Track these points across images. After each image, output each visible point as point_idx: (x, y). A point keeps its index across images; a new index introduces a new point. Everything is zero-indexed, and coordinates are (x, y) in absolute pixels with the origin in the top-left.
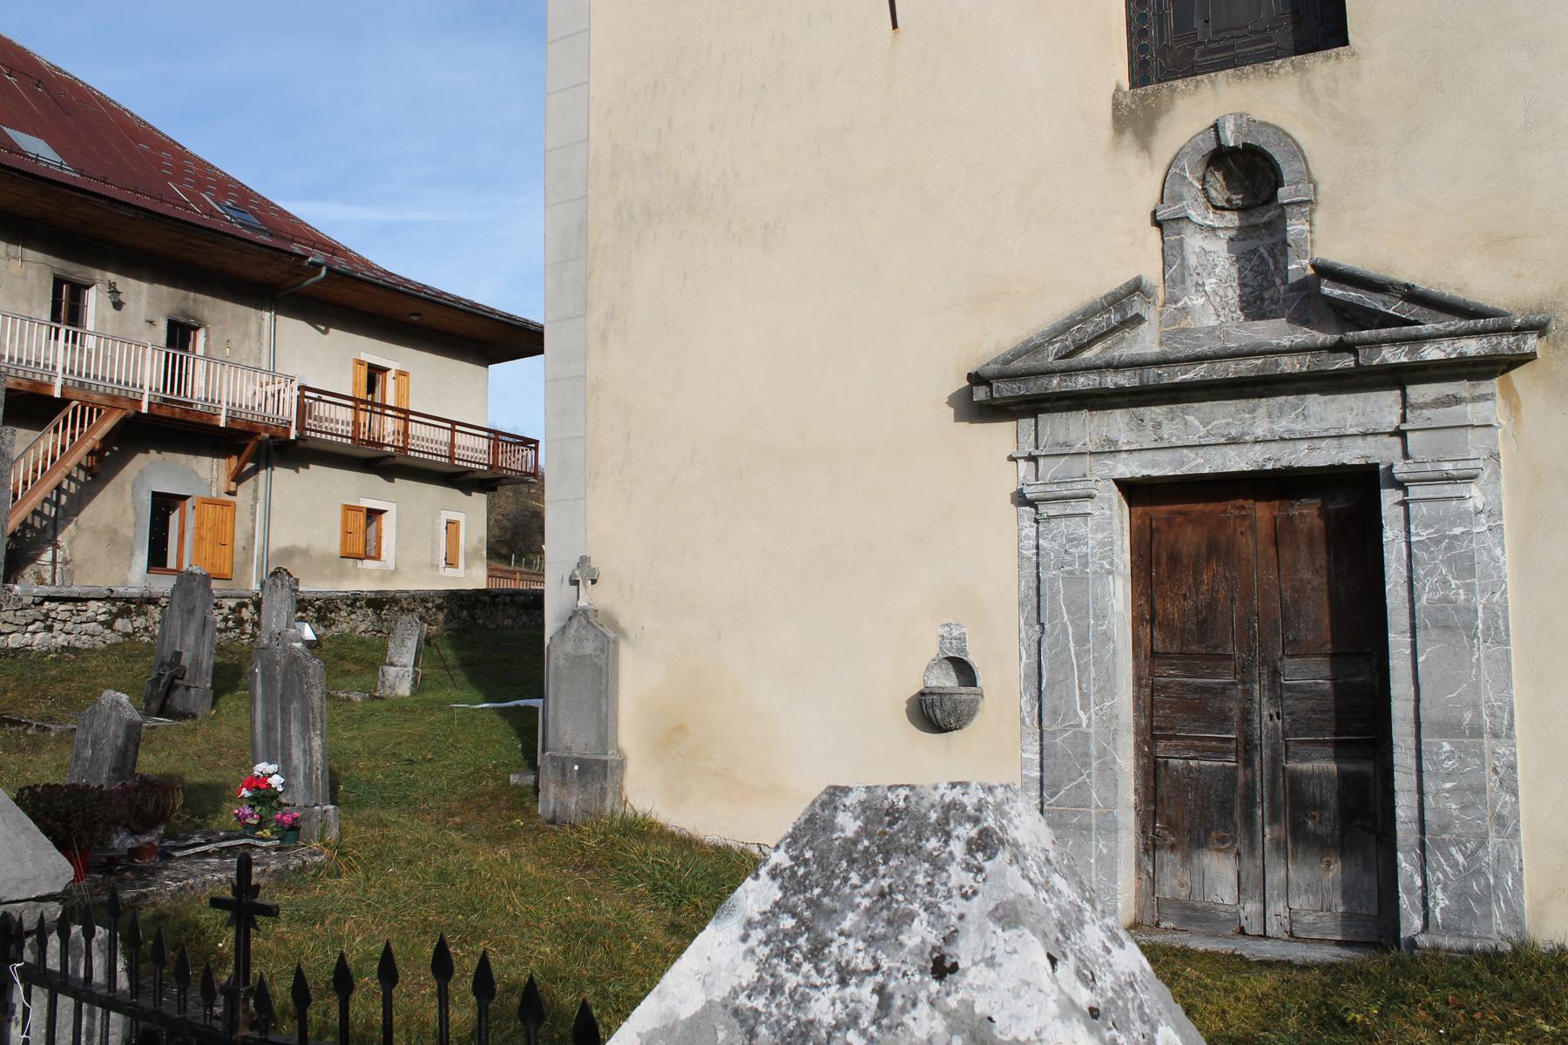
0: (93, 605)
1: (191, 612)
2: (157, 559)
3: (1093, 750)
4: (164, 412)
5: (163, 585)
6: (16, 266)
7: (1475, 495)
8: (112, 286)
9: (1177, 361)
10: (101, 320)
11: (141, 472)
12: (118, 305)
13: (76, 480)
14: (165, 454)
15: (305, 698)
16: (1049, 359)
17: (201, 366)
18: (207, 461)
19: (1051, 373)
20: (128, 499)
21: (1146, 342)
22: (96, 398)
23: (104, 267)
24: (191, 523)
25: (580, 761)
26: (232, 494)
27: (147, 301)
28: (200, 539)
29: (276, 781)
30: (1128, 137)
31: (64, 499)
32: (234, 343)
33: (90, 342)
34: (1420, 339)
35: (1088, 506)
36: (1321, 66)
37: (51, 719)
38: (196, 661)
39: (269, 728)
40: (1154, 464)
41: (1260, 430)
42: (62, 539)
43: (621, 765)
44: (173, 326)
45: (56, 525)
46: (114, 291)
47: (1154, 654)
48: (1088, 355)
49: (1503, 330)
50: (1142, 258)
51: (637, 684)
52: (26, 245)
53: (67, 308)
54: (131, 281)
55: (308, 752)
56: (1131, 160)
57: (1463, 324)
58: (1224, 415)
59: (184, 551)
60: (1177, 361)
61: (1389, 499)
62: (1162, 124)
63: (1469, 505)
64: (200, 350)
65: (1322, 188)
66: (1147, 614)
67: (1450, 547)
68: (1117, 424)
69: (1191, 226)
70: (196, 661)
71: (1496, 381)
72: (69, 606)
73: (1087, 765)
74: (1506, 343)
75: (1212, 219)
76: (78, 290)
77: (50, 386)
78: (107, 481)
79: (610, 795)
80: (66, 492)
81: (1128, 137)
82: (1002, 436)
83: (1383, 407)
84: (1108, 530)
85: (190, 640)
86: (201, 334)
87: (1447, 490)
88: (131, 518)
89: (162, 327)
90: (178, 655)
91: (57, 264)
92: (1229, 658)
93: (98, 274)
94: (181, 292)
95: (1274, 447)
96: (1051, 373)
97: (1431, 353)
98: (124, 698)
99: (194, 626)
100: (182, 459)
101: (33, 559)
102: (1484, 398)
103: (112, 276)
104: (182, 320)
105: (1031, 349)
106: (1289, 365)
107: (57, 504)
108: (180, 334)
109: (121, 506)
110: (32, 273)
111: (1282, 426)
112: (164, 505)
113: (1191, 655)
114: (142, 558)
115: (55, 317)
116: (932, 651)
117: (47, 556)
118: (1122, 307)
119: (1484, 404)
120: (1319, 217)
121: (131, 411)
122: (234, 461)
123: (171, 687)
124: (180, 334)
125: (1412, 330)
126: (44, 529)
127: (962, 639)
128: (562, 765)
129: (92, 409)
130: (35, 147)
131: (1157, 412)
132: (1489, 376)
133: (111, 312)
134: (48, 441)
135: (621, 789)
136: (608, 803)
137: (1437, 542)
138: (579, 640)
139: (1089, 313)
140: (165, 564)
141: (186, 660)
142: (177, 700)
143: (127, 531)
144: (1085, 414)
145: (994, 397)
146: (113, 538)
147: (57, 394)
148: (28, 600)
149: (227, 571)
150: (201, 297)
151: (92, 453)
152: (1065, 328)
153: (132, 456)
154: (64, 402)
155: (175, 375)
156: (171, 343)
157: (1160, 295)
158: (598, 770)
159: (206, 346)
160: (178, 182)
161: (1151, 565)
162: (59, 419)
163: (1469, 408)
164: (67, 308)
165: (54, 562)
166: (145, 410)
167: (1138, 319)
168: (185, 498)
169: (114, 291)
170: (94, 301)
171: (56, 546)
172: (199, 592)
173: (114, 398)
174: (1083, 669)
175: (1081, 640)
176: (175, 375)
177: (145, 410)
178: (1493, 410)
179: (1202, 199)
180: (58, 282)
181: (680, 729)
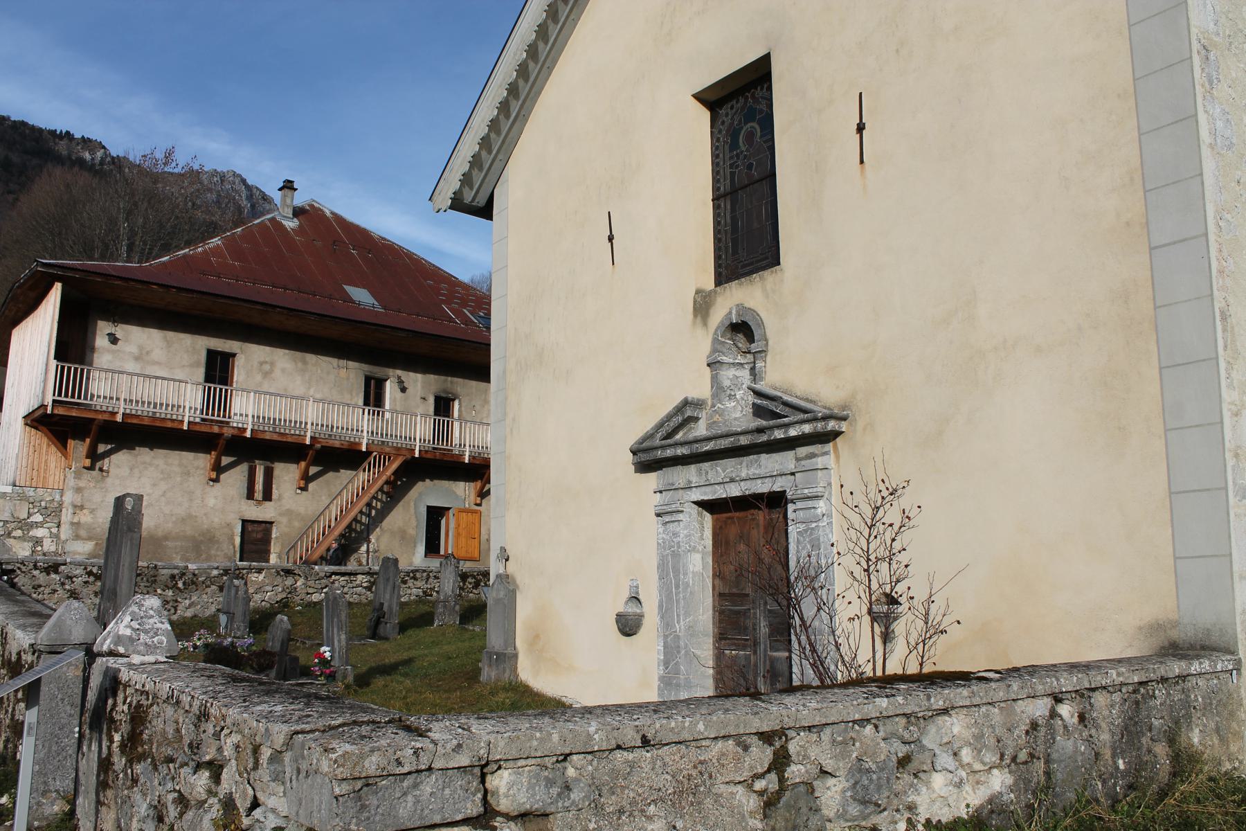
0: (360, 577)
1: (388, 580)
2: (432, 547)
3: (682, 644)
4: (429, 456)
5: (434, 563)
6: (343, 372)
7: (821, 506)
8: (399, 377)
9: (796, 423)
10: (393, 400)
11: (420, 494)
12: (403, 390)
13: (380, 501)
14: (436, 482)
15: (338, 616)
16: (657, 442)
17: (456, 425)
18: (462, 484)
19: (656, 448)
20: (412, 510)
21: (701, 430)
22: (387, 450)
23: (395, 367)
24: (452, 525)
25: (496, 654)
26: (480, 505)
27: (421, 385)
28: (458, 535)
29: (327, 655)
30: (699, 318)
31: (373, 512)
32: (478, 407)
33: (387, 415)
34: (787, 426)
35: (680, 517)
36: (769, 277)
37: (309, 638)
38: (390, 607)
39: (328, 631)
40: (705, 494)
41: (743, 475)
42: (373, 538)
43: (516, 656)
44: (438, 400)
45: (369, 529)
46: (401, 382)
47: (720, 595)
48: (679, 436)
49: (815, 419)
50: (700, 388)
51: (524, 611)
52: (348, 359)
53: (373, 396)
54: (412, 374)
55: (339, 641)
56: (700, 331)
57: (802, 416)
58: (727, 467)
59: (448, 543)
60: (796, 423)
61: (791, 507)
62: (712, 311)
63: (819, 511)
64: (456, 414)
65: (770, 343)
66: (718, 575)
67: (811, 534)
68: (690, 473)
69: (725, 367)
70: (390, 607)
71: (831, 444)
72: (346, 578)
73: (679, 652)
74: (819, 426)
75: (740, 359)
76: (380, 383)
77: (360, 444)
78: (399, 501)
79: (508, 671)
80: (375, 508)
81: (699, 318)
82: (652, 480)
83: (786, 460)
84: (698, 532)
85: (388, 596)
86: (456, 403)
87: (810, 504)
88: (414, 523)
89: (431, 400)
90: (382, 604)
91: (366, 368)
92: (747, 595)
93: (391, 372)
94: (443, 378)
95: (748, 482)
96: (656, 448)
97: (793, 432)
98: (286, 618)
99: (389, 588)
100: (446, 484)
101: (357, 550)
102: (826, 453)
103: (399, 372)
104: (443, 395)
105: (649, 436)
106: (744, 440)
107: (369, 515)
108: (443, 406)
109: (407, 517)
110: (352, 375)
111: (754, 471)
112: (435, 515)
113: (733, 595)
114: (421, 549)
115: (366, 403)
116: (626, 595)
117: (364, 548)
118: (685, 413)
119: (826, 457)
120: (769, 358)
121: (409, 457)
122: (479, 484)
123: (378, 622)
124: (443, 406)
125: (786, 420)
126: (362, 531)
127: (637, 587)
128: (490, 655)
129: (386, 456)
130: (361, 295)
131: (705, 466)
132: (828, 441)
133: (399, 394)
134: (362, 477)
135: (516, 668)
136: (507, 675)
137: (806, 531)
138: (498, 590)
139: (669, 417)
140: (438, 551)
141: (385, 608)
142: (381, 630)
143: (412, 532)
144: (680, 467)
145: (649, 459)
146: (403, 535)
147: (364, 449)
148: (322, 574)
149: (476, 555)
150: (455, 379)
151: (387, 482)
152: (661, 425)
153: (414, 484)
154: (368, 453)
155: (441, 432)
156: (437, 413)
157: (710, 403)
158: (507, 658)
159: (460, 410)
160: (448, 303)
161: (268, 552)
162: (366, 464)
163: (820, 459)
164: (373, 396)
165: (368, 551)
166: (417, 455)
167: (697, 419)
168: (449, 509)
169: (401, 382)
170: (390, 388)
171: (369, 542)
172: (392, 568)
173: (398, 449)
174: (678, 601)
175: (677, 587)
176: (441, 432)
177: (417, 455)
178: (829, 461)
179: (734, 349)
180: (368, 380)
181: (537, 637)
